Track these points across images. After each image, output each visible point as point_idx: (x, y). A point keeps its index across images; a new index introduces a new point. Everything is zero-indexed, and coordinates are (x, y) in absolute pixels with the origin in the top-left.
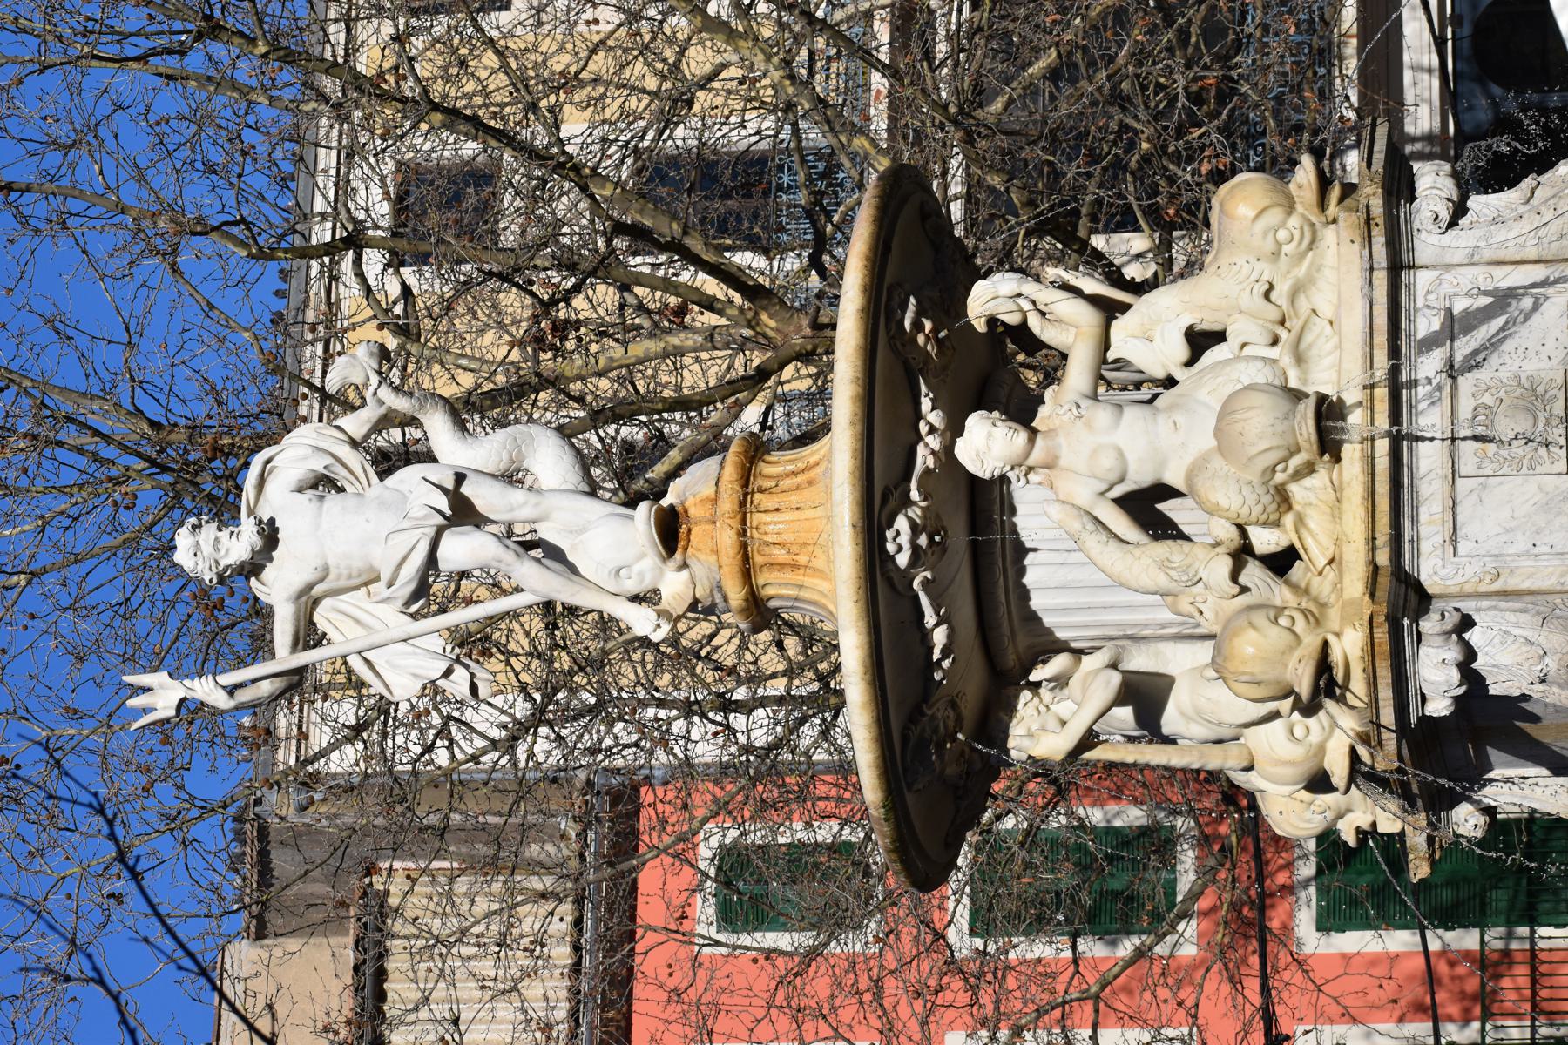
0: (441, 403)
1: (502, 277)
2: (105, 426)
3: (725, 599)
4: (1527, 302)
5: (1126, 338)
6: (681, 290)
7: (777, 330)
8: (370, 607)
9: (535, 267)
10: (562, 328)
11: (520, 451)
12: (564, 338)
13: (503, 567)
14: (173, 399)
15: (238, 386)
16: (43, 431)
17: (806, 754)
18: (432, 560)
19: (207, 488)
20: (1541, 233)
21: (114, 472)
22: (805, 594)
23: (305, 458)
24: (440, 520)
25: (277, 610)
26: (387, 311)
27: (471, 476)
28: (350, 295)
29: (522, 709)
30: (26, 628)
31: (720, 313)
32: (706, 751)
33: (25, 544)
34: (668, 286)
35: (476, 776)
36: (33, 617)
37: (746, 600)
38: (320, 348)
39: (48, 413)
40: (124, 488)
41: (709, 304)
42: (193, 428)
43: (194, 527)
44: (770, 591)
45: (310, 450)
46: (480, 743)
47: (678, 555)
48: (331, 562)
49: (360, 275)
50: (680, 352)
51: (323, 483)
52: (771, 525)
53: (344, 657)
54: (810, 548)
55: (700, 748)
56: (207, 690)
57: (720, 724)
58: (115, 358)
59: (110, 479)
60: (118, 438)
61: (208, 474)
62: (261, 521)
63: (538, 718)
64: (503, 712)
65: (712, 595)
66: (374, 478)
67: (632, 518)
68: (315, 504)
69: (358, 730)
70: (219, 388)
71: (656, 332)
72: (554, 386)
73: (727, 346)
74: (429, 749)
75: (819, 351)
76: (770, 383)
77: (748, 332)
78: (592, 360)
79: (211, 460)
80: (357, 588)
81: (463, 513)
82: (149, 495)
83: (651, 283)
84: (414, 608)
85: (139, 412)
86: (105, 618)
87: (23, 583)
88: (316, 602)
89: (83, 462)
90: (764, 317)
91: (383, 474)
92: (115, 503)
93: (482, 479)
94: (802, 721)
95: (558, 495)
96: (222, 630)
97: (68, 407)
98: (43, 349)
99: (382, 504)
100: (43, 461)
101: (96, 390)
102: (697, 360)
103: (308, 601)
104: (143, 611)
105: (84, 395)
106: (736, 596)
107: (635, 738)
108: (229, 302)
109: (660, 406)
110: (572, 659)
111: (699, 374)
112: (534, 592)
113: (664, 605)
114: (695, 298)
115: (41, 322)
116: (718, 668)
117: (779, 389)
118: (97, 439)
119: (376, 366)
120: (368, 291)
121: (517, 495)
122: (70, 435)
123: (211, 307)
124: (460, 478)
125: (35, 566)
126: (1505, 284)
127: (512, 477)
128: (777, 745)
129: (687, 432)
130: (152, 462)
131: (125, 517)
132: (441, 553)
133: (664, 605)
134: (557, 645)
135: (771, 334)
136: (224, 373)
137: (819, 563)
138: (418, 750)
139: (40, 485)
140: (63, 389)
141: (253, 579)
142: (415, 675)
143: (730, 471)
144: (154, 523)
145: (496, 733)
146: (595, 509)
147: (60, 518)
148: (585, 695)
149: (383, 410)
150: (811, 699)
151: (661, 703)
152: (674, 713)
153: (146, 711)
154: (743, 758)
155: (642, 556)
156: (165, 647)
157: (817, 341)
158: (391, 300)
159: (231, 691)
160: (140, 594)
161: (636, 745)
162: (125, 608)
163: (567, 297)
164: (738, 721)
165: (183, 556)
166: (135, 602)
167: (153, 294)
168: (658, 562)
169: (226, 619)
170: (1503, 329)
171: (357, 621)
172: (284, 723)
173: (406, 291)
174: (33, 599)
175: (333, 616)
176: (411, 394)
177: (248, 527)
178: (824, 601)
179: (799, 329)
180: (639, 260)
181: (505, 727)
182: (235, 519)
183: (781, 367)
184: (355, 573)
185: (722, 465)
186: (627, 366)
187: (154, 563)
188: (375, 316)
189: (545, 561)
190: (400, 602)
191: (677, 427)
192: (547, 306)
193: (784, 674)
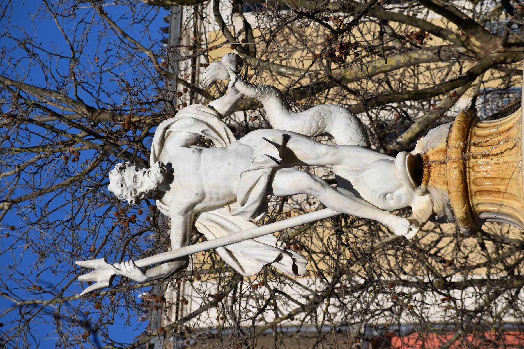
0: (274, 91)
1: (308, 16)
2: (59, 109)
3: (453, 213)
6: (419, 23)
7: (481, 48)
8: (230, 218)
9: (328, 9)
10: (345, 48)
11: (323, 121)
12: (347, 54)
13: (313, 192)
14: (101, 93)
15: (142, 85)
16: (19, 112)
17: (499, 317)
18: (269, 189)
19: (125, 148)
21: (65, 138)
22: (503, 210)
23: (190, 126)
24: (274, 164)
25: (173, 219)
26: (235, 38)
27: (293, 137)
28: (211, 28)
29: (320, 286)
30: (8, 235)
31: (444, 38)
32: (435, 312)
33: (7, 183)
34: (413, 21)
35: (290, 330)
36: (13, 228)
37: (466, 213)
38: (190, 62)
39: (23, 101)
40: (71, 149)
41: (438, 32)
42: (115, 112)
43: (121, 169)
44: (481, 208)
45: (193, 121)
46: (294, 306)
47: (423, 186)
48: (207, 190)
49: (218, 15)
50: (417, 63)
51: (201, 142)
52: (482, 168)
53: (214, 249)
54: (507, 181)
55: (433, 310)
56: (129, 269)
57: (444, 295)
58: (63, 67)
59: (63, 143)
60: (67, 117)
61: (129, 138)
62: (162, 165)
63: (329, 292)
64: (307, 289)
65: (444, 210)
66: (233, 138)
67: (394, 162)
68: (196, 154)
69: (219, 297)
70: (132, 85)
71: (403, 51)
72: (340, 84)
73: (448, 59)
74: (261, 311)
75: (508, 60)
76: (476, 81)
77: (462, 49)
78: (364, 68)
79: (126, 131)
80: (222, 206)
81: (288, 159)
82: (88, 153)
83: (400, 19)
84: (258, 218)
85: (80, 101)
86: (59, 229)
87: (6, 208)
88: (197, 215)
89: (44, 132)
90: (473, 40)
91: (238, 137)
92: (67, 158)
93: (300, 138)
94: (497, 294)
95: (347, 149)
96: (134, 236)
97: (35, 98)
98: (18, 61)
99: (238, 154)
100: (20, 131)
101: (53, 87)
102: (428, 68)
103: (192, 214)
104: (84, 224)
105: (45, 90)
106: (459, 211)
107: (390, 304)
108: (135, 32)
109: (406, 96)
110: (355, 250)
111: (427, 77)
112: (332, 208)
113: (414, 216)
114: (429, 28)
115: (16, 44)
116: (443, 261)
117: (482, 87)
118: (54, 118)
119: (234, 69)
120: (223, 26)
121: (322, 149)
122: (37, 115)
123: (125, 35)
124: (286, 138)
125: (14, 197)
127: (320, 135)
128: (481, 309)
129: (421, 114)
130: (90, 133)
131: (71, 166)
132: (275, 184)
133: (414, 216)
134: (343, 244)
135: (477, 50)
136: (134, 77)
137: (513, 190)
138: (255, 310)
139: (17, 146)
140: (31, 86)
141: (158, 201)
142: (259, 260)
143: (455, 133)
144: (90, 170)
145: (304, 301)
146: (371, 157)
147: (30, 167)
148: (357, 278)
149: (238, 96)
150: (502, 281)
151: (406, 283)
152: (414, 289)
153: (90, 283)
154: (460, 318)
155: (400, 186)
156: (98, 248)
157: (507, 54)
158: (237, 32)
159: (144, 270)
160: (81, 215)
161: (390, 309)
162: (72, 225)
163: (348, 28)
164: (456, 293)
165: (114, 187)
166: (78, 220)
167: (88, 27)
168: (410, 189)
169: (140, 226)
171: (223, 227)
172: (170, 294)
173: (247, 26)
174: (13, 218)
175: (207, 223)
176: (256, 86)
177: (155, 168)
178: (516, 214)
179: (495, 47)
180: (390, 6)
181: (307, 298)
182: (147, 165)
183: (483, 72)
184: (221, 197)
185: (450, 129)
186: (386, 72)
187: (90, 195)
188: (228, 42)
189: (338, 189)
190: (249, 215)
191: (417, 112)
192: (336, 33)
193: (485, 265)
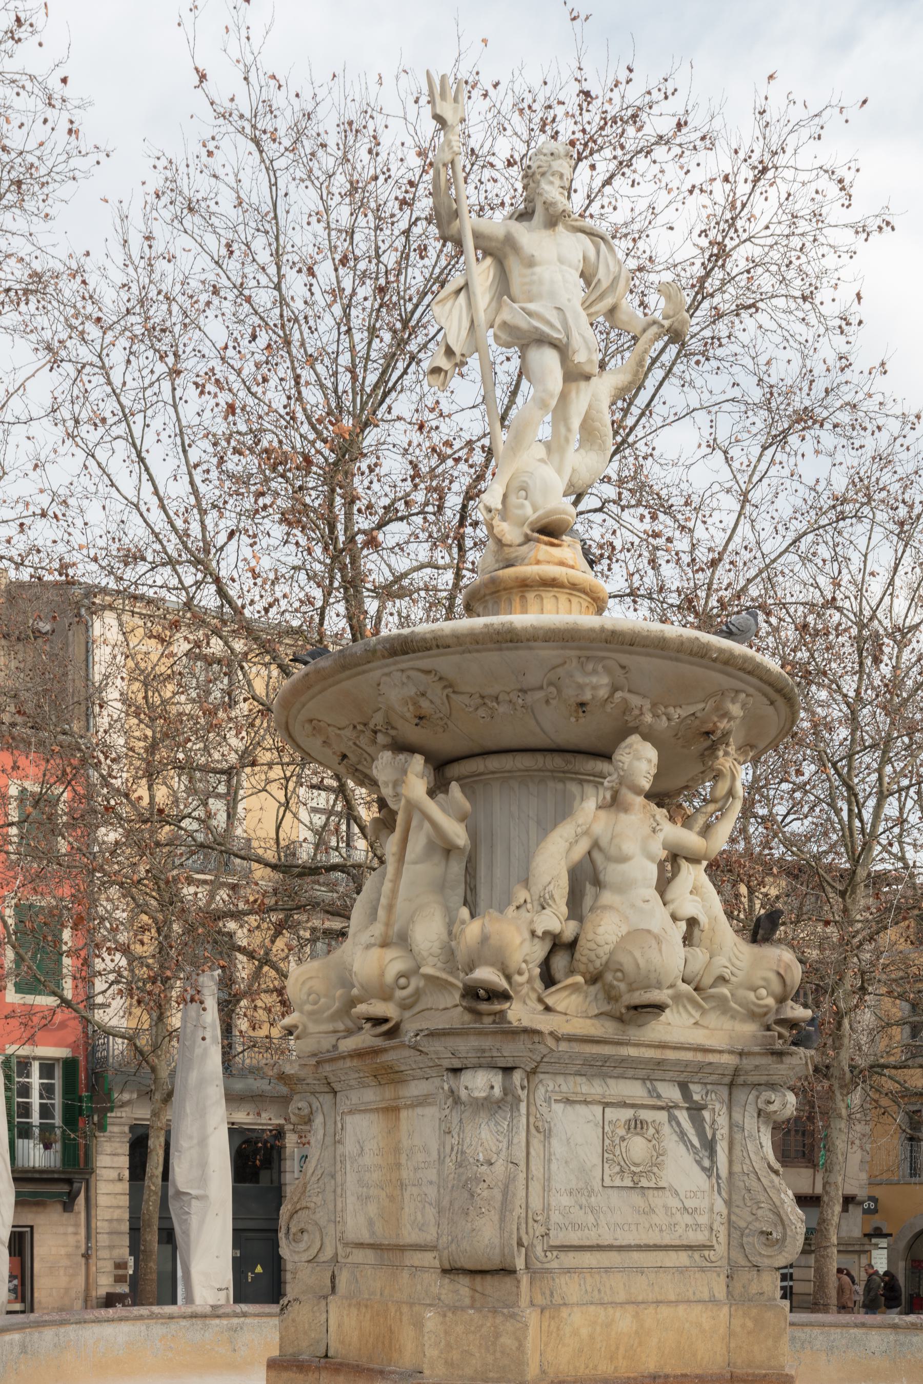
4: (707, 1163)
5: (693, 875)
20: (752, 1175)
48: (537, 269)
126: (719, 1148)
170: (693, 1145)
